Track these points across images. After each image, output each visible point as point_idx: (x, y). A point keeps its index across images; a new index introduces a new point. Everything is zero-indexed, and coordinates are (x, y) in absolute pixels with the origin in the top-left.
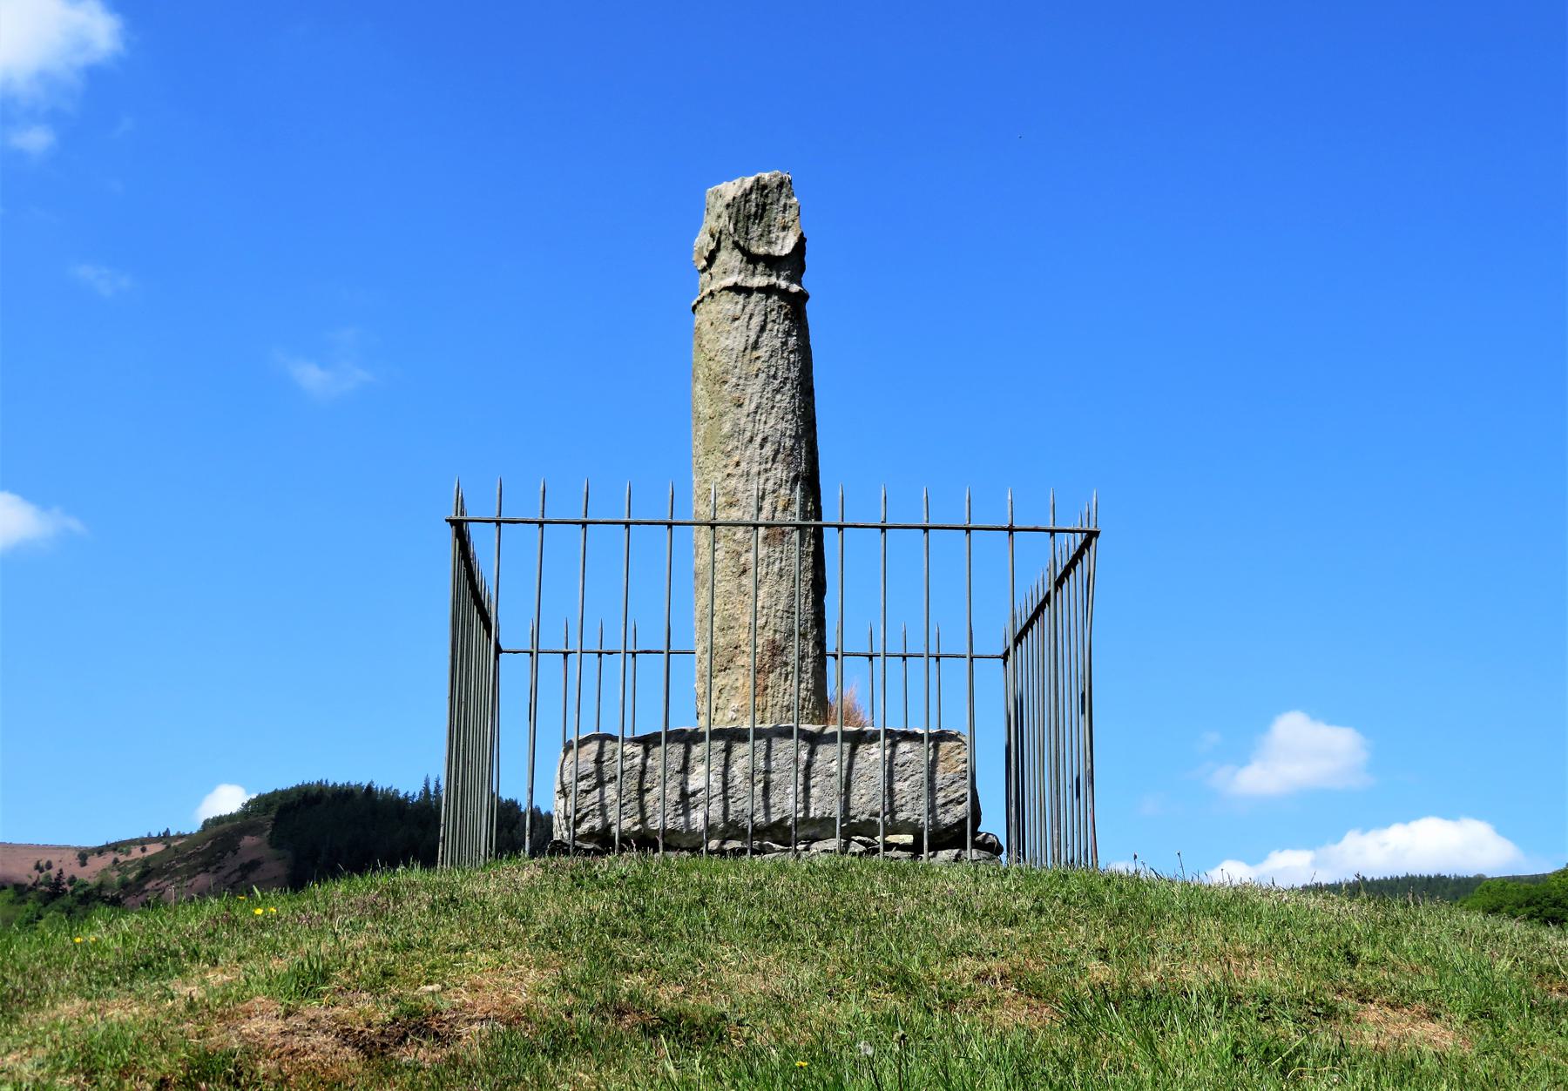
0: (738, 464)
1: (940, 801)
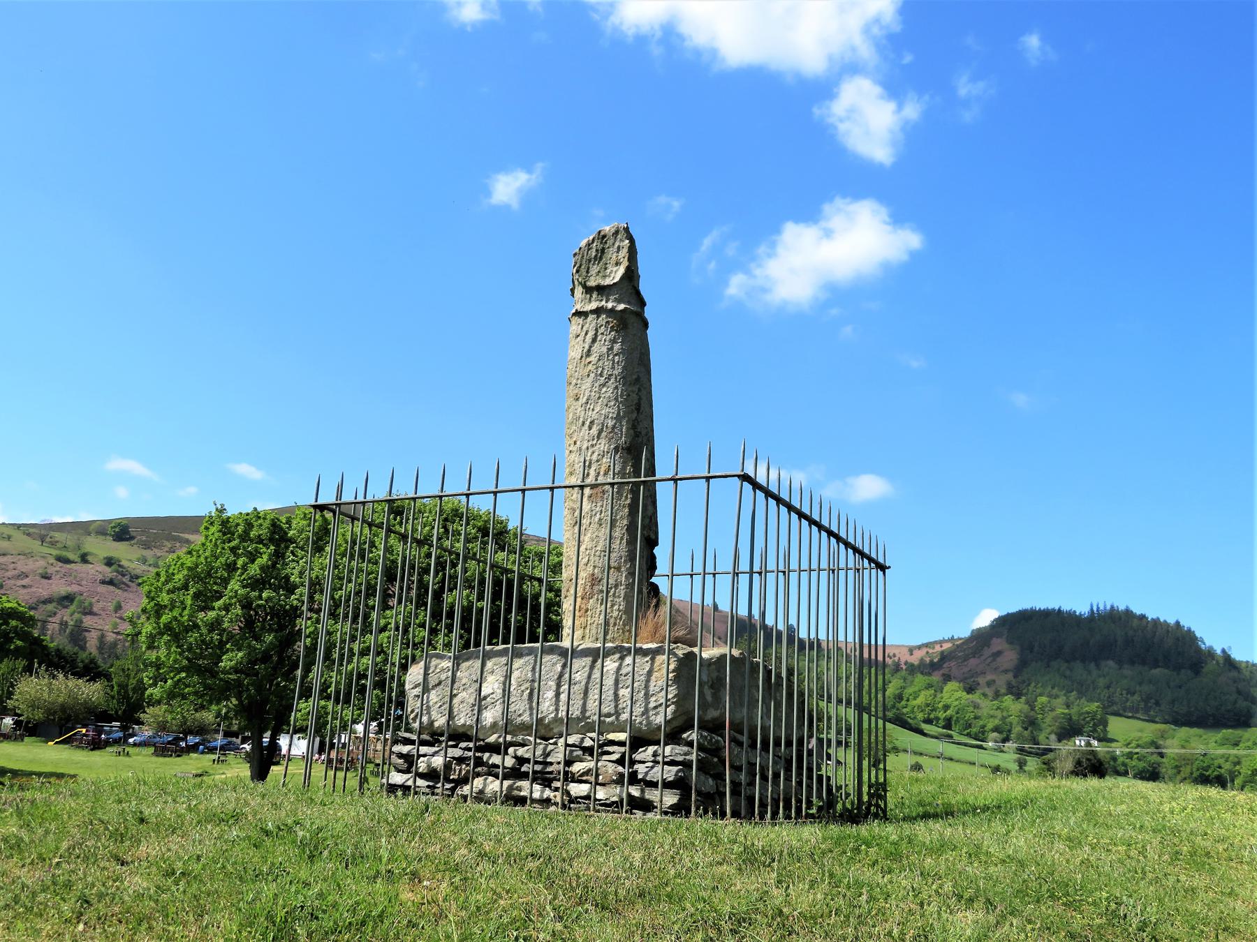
1: (652, 705)
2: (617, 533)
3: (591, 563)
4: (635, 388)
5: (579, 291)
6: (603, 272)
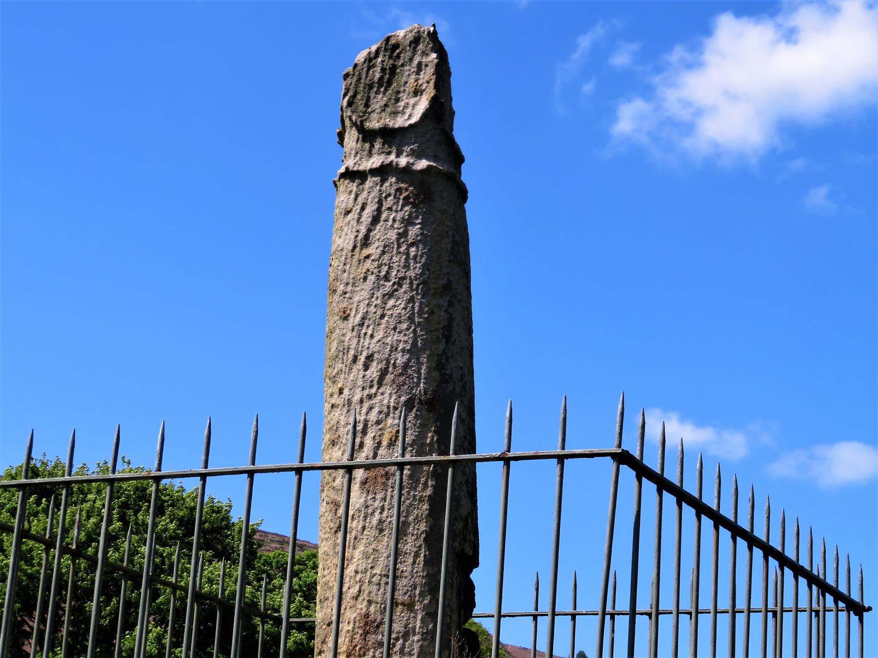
0: (341, 391)
2: (409, 545)
3: (365, 595)
4: (443, 302)
5: (352, 137)
6: (392, 107)
